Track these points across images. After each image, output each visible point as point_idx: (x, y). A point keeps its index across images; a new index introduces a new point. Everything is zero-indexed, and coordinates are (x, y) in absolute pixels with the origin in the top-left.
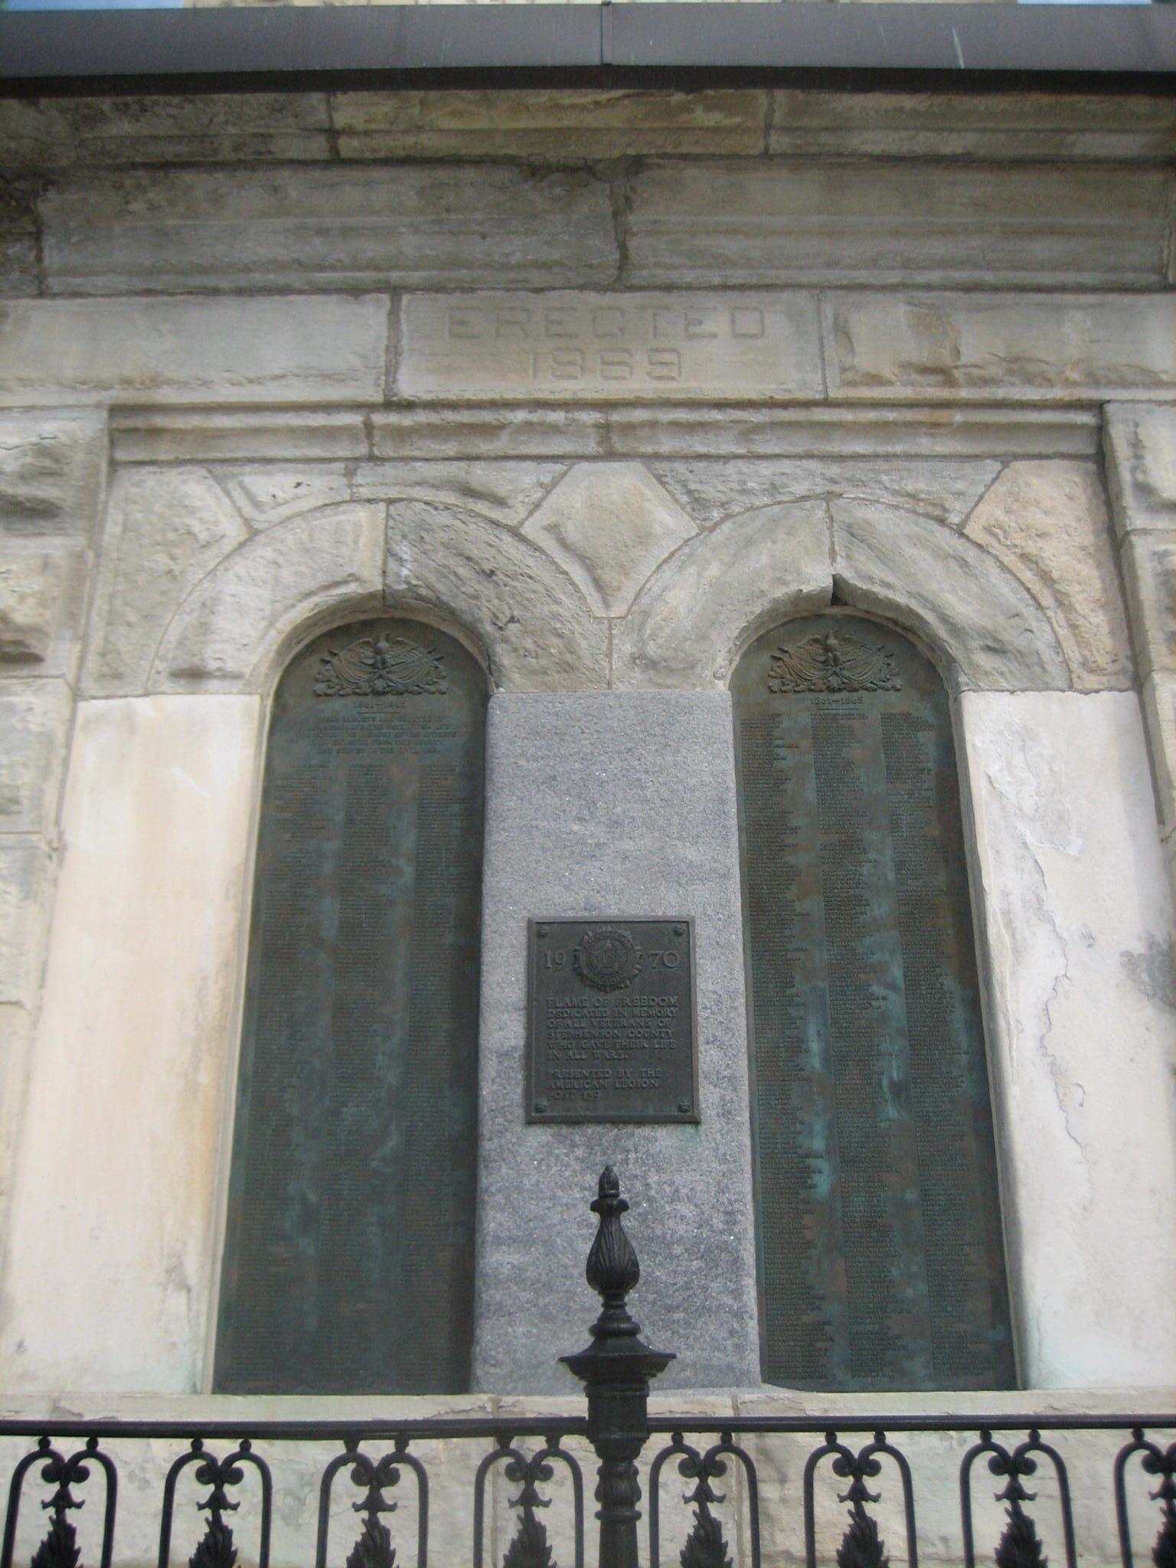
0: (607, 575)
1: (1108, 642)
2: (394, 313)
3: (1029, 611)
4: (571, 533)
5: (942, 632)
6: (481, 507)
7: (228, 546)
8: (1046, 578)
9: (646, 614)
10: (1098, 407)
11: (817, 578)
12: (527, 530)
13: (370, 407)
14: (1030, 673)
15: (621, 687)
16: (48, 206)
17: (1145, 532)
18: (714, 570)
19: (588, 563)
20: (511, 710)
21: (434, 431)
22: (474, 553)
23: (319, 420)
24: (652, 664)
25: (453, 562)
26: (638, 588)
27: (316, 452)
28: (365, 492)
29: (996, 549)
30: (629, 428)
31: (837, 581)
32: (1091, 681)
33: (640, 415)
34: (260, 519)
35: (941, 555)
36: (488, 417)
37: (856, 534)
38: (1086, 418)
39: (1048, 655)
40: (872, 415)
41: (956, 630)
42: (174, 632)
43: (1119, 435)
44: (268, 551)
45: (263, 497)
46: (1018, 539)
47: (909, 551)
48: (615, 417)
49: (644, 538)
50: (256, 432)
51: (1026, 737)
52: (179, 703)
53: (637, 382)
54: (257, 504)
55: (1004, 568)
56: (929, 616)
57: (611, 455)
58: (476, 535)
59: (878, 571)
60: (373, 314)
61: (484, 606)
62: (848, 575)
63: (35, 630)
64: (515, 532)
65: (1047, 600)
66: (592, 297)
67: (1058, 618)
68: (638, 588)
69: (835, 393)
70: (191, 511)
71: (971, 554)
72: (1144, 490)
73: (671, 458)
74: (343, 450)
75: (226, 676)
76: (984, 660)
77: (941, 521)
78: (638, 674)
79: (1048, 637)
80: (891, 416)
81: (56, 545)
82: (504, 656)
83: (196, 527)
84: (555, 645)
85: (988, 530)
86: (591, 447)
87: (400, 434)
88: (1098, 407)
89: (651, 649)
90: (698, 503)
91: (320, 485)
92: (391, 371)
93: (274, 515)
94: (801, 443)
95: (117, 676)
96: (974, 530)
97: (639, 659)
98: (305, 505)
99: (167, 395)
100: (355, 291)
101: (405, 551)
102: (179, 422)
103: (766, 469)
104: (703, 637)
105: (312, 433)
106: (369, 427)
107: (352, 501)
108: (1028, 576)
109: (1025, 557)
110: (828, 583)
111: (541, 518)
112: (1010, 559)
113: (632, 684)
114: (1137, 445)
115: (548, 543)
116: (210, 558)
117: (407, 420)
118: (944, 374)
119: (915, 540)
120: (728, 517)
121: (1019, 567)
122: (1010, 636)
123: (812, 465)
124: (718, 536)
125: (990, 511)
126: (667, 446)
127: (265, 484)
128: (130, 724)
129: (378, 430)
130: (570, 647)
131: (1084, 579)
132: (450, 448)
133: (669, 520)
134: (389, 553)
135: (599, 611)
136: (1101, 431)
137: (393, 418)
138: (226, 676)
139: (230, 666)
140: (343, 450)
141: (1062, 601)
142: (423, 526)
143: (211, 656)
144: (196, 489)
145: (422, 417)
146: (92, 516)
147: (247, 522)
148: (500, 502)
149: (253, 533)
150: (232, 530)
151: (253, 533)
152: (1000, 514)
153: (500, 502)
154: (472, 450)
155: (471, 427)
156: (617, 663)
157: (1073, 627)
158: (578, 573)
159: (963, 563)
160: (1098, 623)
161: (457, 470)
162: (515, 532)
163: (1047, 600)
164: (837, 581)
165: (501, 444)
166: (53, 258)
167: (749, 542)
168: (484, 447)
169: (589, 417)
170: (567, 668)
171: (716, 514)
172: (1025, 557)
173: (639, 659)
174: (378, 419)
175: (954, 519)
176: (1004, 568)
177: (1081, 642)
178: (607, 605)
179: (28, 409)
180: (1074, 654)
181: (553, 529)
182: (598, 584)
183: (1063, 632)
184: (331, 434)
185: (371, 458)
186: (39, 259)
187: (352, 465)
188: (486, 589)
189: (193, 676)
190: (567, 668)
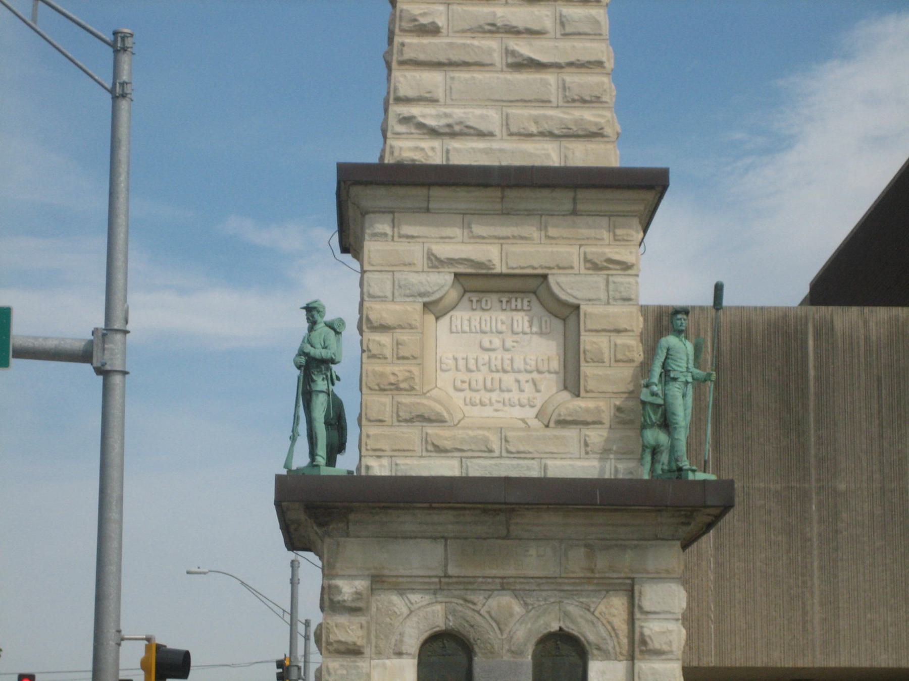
0: (502, 627)
1: (627, 647)
2: (446, 546)
3: (608, 638)
4: (493, 614)
5: (586, 643)
6: (470, 605)
7: (405, 615)
8: (614, 629)
9: (512, 638)
10: (633, 579)
11: (555, 627)
12: (482, 612)
13: (440, 577)
14: (606, 655)
15: (505, 658)
16: (352, 517)
17: (639, 619)
18: (529, 626)
19: (498, 624)
20: (479, 661)
21: (457, 583)
22: (468, 619)
23: (427, 580)
24: (513, 652)
25: (463, 622)
26: (511, 625)
27: (426, 587)
28: (440, 599)
29: (602, 619)
30: (508, 583)
31: (561, 629)
32: (621, 658)
33: (512, 580)
34: (412, 608)
35: (587, 621)
36: (472, 580)
37: (566, 614)
38: (629, 581)
39: (611, 650)
40: (572, 581)
41: (588, 643)
42: (393, 641)
43: (636, 588)
44: (416, 615)
45: (413, 601)
46: (607, 616)
47: (580, 620)
48: (505, 581)
49: (511, 615)
50: (410, 582)
51: (603, 673)
52: (396, 661)
53: (510, 571)
54: (412, 604)
55: (603, 625)
56: (582, 639)
57: (503, 589)
58: (469, 613)
59: (571, 626)
60: (439, 548)
61: (472, 635)
62: (563, 626)
63: (363, 647)
64: (478, 612)
65: (613, 634)
66: (500, 541)
67: (615, 639)
68: (511, 625)
69: (563, 575)
70: (394, 605)
71: (595, 620)
72: (640, 608)
73: (520, 590)
74: (433, 587)
75: (407, 654)
76: (595, 652)
77: (589, 610)
78: (509, 654)
79: (612, 645)
80: (577, 581)
81: (363, 619)
82: (477, 649)
83: (396, 610)
84: (489, 646)
85: (600, 614)
86: (499, 587)
87: (448, 584)
88: (633, 579)
89: (513, 648)
90: (526, 604)
91: (427, 598)
92: (446, 566)
93: (416, 606)
94: (553, 587)
95: (380, 653)
96: (597, 613)
97: (509, 651)
98: (424, 603)
99: (386, 572)
100: (434, 538)
101: (450, 617)
102: (390, 580)
103: (544, 594)
104: (525, 645)
105: (425, 583)
106: (440, 582)
107: (436, 602)
108: (609, 627)
109: (609, 622)
110: (558, 628)
111: (486, 608)
112: (605, 622)
113: (507, 658)
114: (640, 593)
115: (487, 616)
116: (401, 619)
117: (450, 580)
118: (592, 571)
119: (581, 616)
120: (533, 608)
121: (607, 625)
122: (603, 646)
123: (556, 592)
124: (531, 614)
125: (602, 607)
126: (518, 587)
127: (415, 598)
128: (384, 666)
129: (441, 585)
130: (493, 647)
131: (622, 627)
132: (462, 587)
133: (518, 609)
134: (447, 618)
135: (500, 636)
136: (633, 586)
137: (447, 580)
138: (407, 654)
139: (409, 652)
140: (433, 587)
141: (617, 635)
142: (455, 611)
143: (404, 649)
144: (395, 598)
145: (454, 580)
146: (368, 608)
147: (409, 608)
148: (474, 604)
149: (411, 612)
150: (405, 611)
151: (411, 612)
152: (604, 610)
153: (474, 604)
154: (444, 235)
155: (468, 584)
156: (504, 651)
157: (619, 643)
158: (494, 625)
159: (593, 624)
160: (625, 641)
161: (462, 593)
162: (478, 612)
163: (613, 634)
164: (561, 629)
165: (475, 586)
166: (352, 528)
167: (539, 617)
168: (470, 587)
169: (498, 581)
170: (492, 653)
171: (530, 607)
172: (609, 622)
173: (509, 651)
174: (443, 580)
175: (592, 610)
176: (603, 625)
177: (620, 648)
178: (502, 634)
179: (349, 576)
180: (618, 649)
181: (489, 612)
182: (500, 629)
183: (616, 644)
184: (429, 583)
185: (441, 589)
186: (348, 528)
187: (435, 594)
188: (471, 630)
189: (399, 654)
190: (492, 653)
